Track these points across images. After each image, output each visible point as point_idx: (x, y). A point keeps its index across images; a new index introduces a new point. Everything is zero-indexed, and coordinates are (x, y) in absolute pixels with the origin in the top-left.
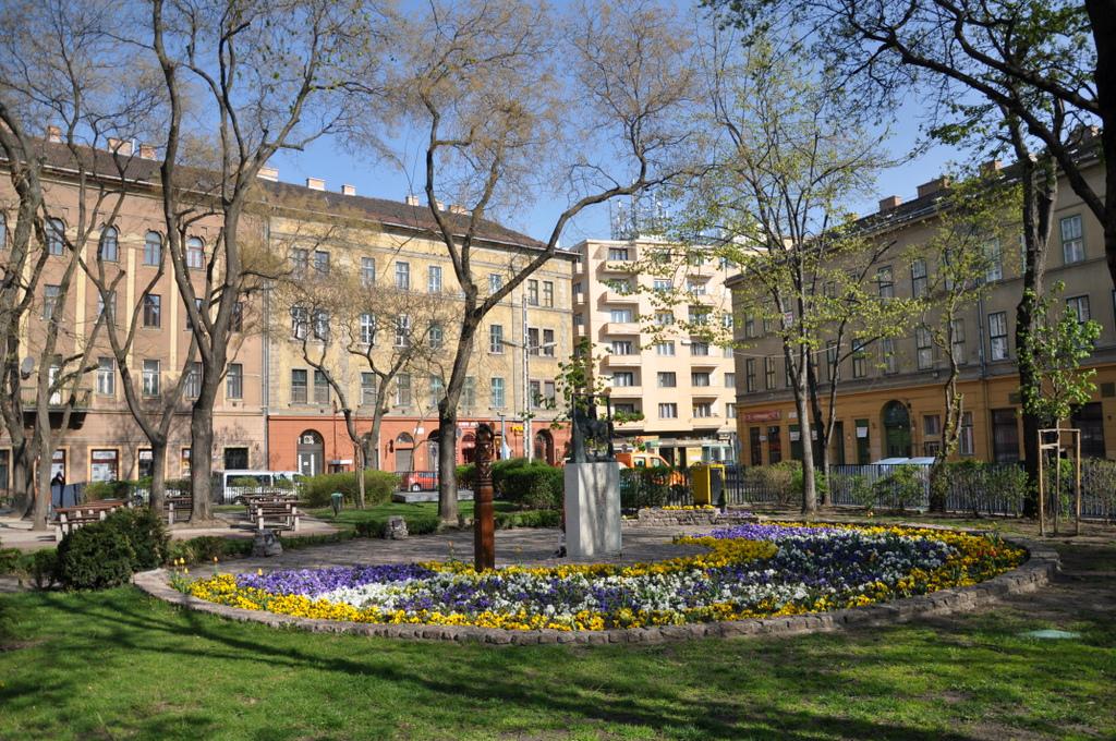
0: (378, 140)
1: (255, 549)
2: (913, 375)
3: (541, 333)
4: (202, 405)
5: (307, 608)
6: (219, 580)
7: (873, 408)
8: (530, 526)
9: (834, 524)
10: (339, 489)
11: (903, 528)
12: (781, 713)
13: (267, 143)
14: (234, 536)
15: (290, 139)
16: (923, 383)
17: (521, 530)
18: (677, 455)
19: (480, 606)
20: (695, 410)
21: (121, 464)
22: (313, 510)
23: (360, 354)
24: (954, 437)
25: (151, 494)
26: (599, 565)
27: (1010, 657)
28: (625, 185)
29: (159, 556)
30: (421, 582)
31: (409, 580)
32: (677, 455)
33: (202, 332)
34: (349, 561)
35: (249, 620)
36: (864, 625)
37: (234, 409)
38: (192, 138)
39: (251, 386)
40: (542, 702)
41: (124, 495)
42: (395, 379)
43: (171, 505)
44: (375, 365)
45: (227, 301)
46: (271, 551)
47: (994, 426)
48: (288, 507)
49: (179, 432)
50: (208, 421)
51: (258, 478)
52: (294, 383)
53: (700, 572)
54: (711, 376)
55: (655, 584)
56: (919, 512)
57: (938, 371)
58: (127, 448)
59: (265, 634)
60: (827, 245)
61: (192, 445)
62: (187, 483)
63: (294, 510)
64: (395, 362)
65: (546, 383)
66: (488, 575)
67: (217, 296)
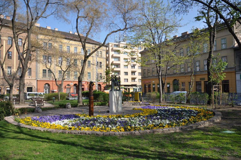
0: (64, 17)
1: (35, 111)
2: (180, 74)
3: (99, 63)
4: (22, 77)
5: (50, 126)
6: (27, 118)
7: (171, 81)
8: (99, 105)
9: (167, 105)
10: (54, 97)
11: (183, 107)
12: (177, 154)
13: (38, 16)
14: (30, 108)
15: (43, 15)
16: (182, 75)
17: (97, 106)
18: (128, 90)
19: (92, 125)
20: (132, 81)
21: (2, 90)
22: (48, 101)
23: (59, 66)
24: (192, 87)
25: (9, 98)
26: (118, 115)
27: (223, 138)
28: (122, 29)
29: (12, 112)
30: (77, 119)
31: (74, 118)
32: (128, 90)
33: (22, 60)
34: (58, 113)
35: (35, 129)
36: (186, 130)
37: (29, 78)
38: (19, 14)
39: (33, 73)
40: (116, 152)
41: (3, 98)
42: (67, 72)
43: (14, 100)
44: (62, 69)
45: (28, 53)
46: (39, 111)
47: (197, 85)
48: (42, 101)
49: (16, 83)
50: (23, 80)
51: (35, 94)
52: (43, 73)
53: (142, 117)
54: (135, 73)
55: (133, 120)
56: (184, 103)
57: (185, 73)
58: (3, 87)
59: (40, 133)
60: (166, 44)
61: (20, 86)
62: (18, 95)
63: (44, 101)
64: (67, 68)
65: (100, 74)
66: (92, 117)
67: (25, 52)
